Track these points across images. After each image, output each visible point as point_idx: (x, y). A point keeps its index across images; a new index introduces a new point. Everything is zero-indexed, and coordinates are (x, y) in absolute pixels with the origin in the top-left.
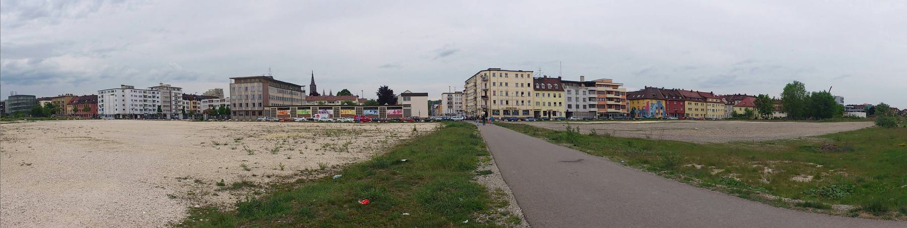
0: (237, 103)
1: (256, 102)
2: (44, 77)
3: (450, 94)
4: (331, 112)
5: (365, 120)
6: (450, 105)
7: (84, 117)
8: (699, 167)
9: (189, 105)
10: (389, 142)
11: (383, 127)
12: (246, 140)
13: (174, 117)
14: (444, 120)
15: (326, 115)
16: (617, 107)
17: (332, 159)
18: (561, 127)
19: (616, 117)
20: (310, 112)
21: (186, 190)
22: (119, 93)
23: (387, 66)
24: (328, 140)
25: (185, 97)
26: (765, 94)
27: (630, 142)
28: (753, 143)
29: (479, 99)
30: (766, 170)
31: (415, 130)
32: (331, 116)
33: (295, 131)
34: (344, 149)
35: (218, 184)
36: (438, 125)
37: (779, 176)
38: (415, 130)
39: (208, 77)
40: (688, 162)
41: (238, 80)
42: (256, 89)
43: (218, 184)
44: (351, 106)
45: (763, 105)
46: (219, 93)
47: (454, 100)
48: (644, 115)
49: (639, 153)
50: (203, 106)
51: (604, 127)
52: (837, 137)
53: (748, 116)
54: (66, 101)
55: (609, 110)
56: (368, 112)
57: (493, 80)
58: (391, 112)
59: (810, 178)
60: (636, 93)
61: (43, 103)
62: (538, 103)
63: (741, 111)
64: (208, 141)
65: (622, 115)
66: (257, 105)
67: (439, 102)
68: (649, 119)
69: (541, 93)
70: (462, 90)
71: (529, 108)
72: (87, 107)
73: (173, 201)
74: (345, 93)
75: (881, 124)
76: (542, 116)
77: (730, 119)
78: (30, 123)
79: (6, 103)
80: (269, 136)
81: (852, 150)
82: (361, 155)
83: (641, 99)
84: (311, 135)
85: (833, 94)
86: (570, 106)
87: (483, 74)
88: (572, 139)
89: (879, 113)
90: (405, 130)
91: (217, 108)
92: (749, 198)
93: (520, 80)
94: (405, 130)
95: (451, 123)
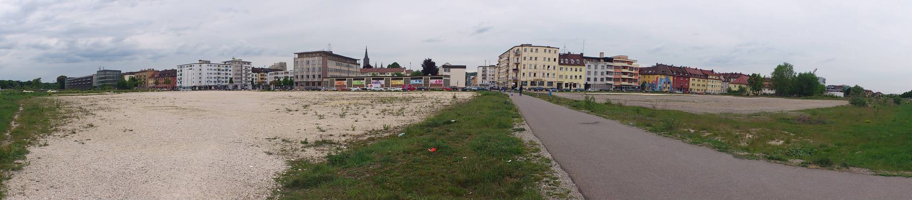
0: (299, 75)
1: (316, 74)
2: (125, 54)
3: (485, 68)
4: (383, 82)
5: (411, 89)
6: (484, 77)
7: (161, 89)
8: (692, 131)
9: (257, 77)
10: (436, 107)
11: (428, 94)
12: (312, 107)
13: (244, 88)
14: (479, 90)
15: (379, 85)
16: (630, 80)
17: (393, 122)
18: (580, 97)
19: (628, 89)
20: (364, 82)
21: (278, 147)
22: (197, 67)
23: (429, 41)
24: (384, 106)
25: (255, 70)
26: (757, 73)
27: (638, 110)
28: (740, 115)
29: (511, 71)
30: (748, 136)
31: (454, 97)
32: (382, 86)
33: (354, 99)
34: (401, 112)
35: (302, 143)
36: (475, 94)
37: (758, 140)
38: (454, 97)
39: (275, 52)
40: (685, 127)
41: (301, 55)
42: (316, 62)
43: (302, 143)
44: (399, 77)
45: (755, 83)
46: (283, 66)
47: (488, 73)
48: (653, 89)
49: (647, 119)
50: (270, 78)
51: (618, 97)
52: (814, 112)
53: (740, 93)
54: (148, 75)
55: (623, 83)
56: (413, 82)
57: (524, 54)
58: (433, 81)
59: (782, 142)
60: (648, 69)
61: (127, 78)
62: (561, 76)
63: (735, 88)
64: (282, 108)
65: (634, 87)
66: (317, 77)
67: (475, 74)
68: (657, 92)
69: (564, 67)
70: (495, 64)
71: (553, 80)
72: (167, 80)
73: (271, 157)
74: (395, 65)
75: (854, 103)
76: (564, 87)
77: (725, 94)
78: (116, 95)
79: (95, 78)
80: (333, 103)
81: (824, 123)
82: (415, 118)
83: (651, 74)
84: (368, 102)
85: (818, 75)
86: (589, 79)
87: (516, 49)
88: (589, 106)
89: (854, 94)
90: (446, 97)
91: (282, 80)
92: (727, 152)
93: (547, 55)
94: (446, 97)
95: (485, 92)
